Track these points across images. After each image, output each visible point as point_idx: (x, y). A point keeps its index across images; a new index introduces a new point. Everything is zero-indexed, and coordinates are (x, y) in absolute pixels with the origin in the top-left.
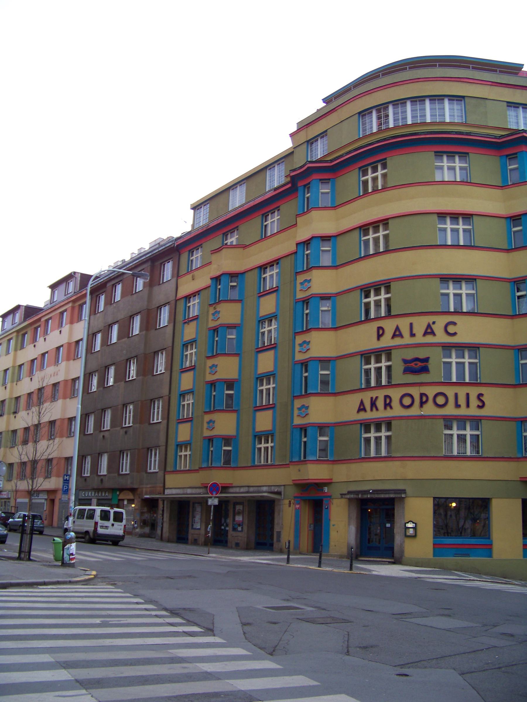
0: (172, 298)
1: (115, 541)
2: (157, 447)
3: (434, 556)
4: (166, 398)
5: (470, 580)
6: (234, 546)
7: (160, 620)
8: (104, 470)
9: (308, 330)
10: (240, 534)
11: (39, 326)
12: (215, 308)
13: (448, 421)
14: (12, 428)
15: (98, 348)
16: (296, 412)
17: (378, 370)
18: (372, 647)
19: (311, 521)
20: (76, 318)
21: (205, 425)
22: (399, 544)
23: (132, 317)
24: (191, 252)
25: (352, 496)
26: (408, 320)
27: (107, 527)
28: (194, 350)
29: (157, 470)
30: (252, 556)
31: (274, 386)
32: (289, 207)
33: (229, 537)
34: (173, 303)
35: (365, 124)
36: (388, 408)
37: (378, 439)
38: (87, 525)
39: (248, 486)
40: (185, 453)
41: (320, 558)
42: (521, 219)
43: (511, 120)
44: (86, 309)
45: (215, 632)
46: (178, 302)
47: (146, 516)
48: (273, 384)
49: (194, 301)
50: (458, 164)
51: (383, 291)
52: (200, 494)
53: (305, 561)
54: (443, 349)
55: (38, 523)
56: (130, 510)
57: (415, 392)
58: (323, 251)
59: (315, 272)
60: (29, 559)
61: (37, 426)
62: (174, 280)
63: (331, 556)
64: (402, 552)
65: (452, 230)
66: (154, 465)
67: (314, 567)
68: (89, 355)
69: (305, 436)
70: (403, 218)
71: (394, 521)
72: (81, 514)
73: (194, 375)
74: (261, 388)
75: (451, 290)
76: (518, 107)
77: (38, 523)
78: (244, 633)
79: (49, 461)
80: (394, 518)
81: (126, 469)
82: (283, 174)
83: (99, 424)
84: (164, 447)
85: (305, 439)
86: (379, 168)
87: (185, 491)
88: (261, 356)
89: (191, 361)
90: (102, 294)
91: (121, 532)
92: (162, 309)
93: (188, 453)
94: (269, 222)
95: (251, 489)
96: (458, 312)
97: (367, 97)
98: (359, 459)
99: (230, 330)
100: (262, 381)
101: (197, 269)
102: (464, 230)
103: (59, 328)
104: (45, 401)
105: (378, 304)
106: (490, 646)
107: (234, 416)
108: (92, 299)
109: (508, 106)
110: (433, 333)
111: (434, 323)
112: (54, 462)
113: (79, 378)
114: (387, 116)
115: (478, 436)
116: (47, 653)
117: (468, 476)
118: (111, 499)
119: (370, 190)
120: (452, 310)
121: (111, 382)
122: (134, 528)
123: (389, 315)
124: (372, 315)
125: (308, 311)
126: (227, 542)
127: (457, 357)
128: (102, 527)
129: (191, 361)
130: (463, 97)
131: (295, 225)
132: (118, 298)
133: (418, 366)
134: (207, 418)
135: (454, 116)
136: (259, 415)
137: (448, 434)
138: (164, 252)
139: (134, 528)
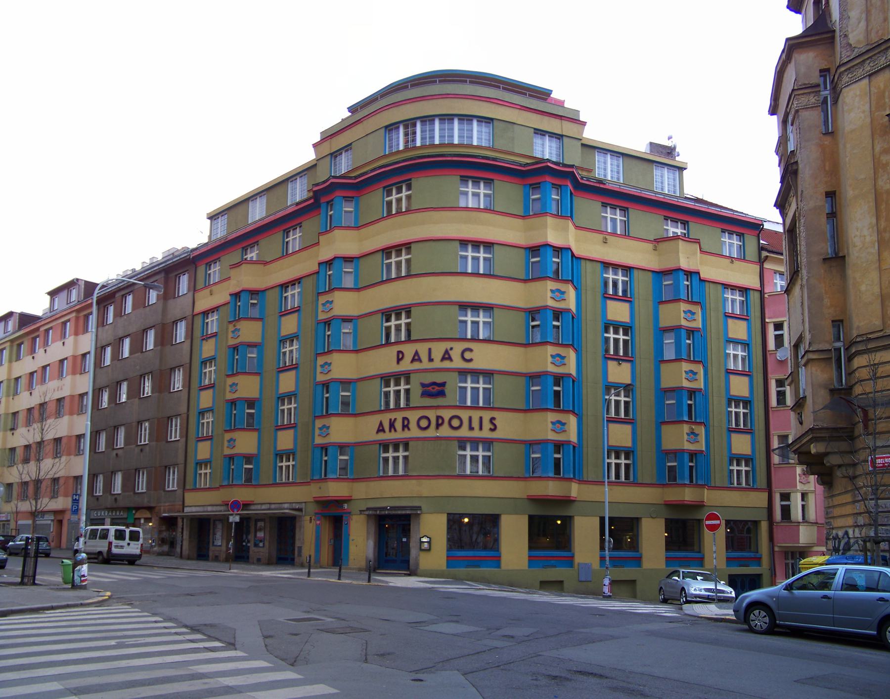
0: (188, 313)
1: (131, 560)
2: (175, 465)
3: (448, 567)
4: (185, 416)
7: (180, 638)
8: (118, 489)
9: (330, 352)
10: (261, 550)
11: (38, 336)
13: (462, 443)
14: (10, 446)
15: (108, 362)
16: (317, 432)
17: (397, 393)
18: (389, 654)
20: (81, 328)
21: (226, 444)
23: (145, 331)
24: (208, 265)
27: (122, 547)
28: (213, 368)
29: (175, 488)
32: (311, 224)
33: (251, 552)
34: (190, 317)
37: (396, 459)
38: (101, 546)
41: (340, 571)
44: (93, 320)
45: (237, 646)
46: (196, 318)
47: (165, 534)
50: (482, 190)
55: (43, 545)
56: (147, 529)
57: (432, 414)
58: (345, 272)
59: (337, 294)
60: (34, 584)
61: (40, 444)
63: (351, 569)
64: (417, 564)
65: (473, 258)
66: (172, 483)
68: (98, 369)
69: (326, 455)
70: (428, 244)
72: (93, 534)
73: (214, 393)
75: (611, 276)
77: (43, 545)
78: (266, 646)
79: (55, 480)
81: (142, 487)
83: (111, 442)
85: (326, 458)
87: (205, 509)
88: (283, 376)
89: (210, 379)
90: (110, 304)
91: (138, 552)
93: (208, 471)
94: (290, 238)
95: (273, 506)
96: (475, 339)
100: (283, 401)
101: (215, 284)
102: (485, 259)
103: (61, 339)
104: (49, 417)
108: (99, 309)
110: (450, 359)
111: (451, 349)
112: (61, 482)
113: (87, 393)
114: (415, 133)
115: (489, 457)
116: (55, 680)
117: (482, 493)
118: (126, 519)
120: (469, 336)
121: (124, 398)
122: (152, 546)
123: (409, 340)
126: (248, 558)
128: (116, 547)
129: (210, 379)
130: (492, 119)
131: (318, 244)
132: (129, 309)
134: (227, 436)
139: (152, 546)
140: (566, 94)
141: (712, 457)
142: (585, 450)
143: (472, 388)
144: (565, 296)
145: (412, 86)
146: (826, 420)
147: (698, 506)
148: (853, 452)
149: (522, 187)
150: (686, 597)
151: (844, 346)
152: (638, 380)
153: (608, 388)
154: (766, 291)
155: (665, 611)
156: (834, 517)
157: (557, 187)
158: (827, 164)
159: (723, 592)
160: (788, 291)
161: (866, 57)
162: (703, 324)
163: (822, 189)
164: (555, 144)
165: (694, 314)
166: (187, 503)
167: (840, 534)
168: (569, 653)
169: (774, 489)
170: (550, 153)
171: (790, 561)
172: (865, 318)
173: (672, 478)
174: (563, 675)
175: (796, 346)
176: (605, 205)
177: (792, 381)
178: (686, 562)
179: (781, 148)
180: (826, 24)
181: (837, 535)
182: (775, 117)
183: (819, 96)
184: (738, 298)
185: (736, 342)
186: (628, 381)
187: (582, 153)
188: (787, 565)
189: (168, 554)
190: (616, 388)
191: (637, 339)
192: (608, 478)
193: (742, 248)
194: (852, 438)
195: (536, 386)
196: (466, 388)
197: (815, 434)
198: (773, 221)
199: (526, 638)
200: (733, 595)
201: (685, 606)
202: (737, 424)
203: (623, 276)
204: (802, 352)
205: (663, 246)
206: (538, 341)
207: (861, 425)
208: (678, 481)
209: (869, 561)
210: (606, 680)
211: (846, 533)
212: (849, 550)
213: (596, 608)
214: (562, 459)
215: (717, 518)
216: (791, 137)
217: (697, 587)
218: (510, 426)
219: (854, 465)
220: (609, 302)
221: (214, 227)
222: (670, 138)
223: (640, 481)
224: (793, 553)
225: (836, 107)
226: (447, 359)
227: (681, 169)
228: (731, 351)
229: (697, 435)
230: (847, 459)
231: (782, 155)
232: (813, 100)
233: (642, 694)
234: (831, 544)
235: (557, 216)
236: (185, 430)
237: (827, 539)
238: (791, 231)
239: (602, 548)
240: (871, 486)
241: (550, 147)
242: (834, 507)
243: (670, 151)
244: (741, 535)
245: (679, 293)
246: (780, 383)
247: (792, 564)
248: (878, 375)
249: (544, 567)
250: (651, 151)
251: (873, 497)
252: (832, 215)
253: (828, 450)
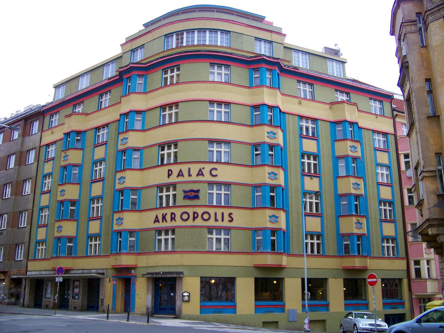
0: (37, 145)
3: (201, 313)
4: (31, 211)
6: (73, 309)
9: (125, 170)
10: (77, 301)
12: (65, 153)
13: (210, 230)
16: (115, 222)
17: (168, 197)
19: (123, 292)
21: (56, 229)
23: (9, 156)
24: (52, 116)
26: (188, 166)
29: (22, 259)
30: (84, 315)
31: (102, 204)
32: (117, 91)
33: (70, 303)
37: (166, 240)
39: (83, 269)
40: (42, 248)
41: (128, 316)
46: (41, 148)
47: (13, 290)
48: (101, 203)
49: (52, 148)
50: (223, 71)
51: (173, 147)
52: (51, 274)
53: (119, 318)
57: (190, 211)
59: (130, 133)
62: (40, 133)
63: (136, 314)
64: (181, 311)
65: (218, 112)
66: (20, 256)
67: (125, 321)
69: (120, 237)
74: (93, 206)
75: (215, 148)
82: (115, 69)
84: (28, 243)
85: (120, 239)
86: (175, 70)
87: (41, 273)
88: (94, 185)
92: (31, 152)
93: (44, 247)
94: (103, 99)
95: (85, 271)
96: (219, 162)
99: (75, 168)
102: (225, 112)
107: (75, 223)
111: (203, 168)
114: (183, 38)
115: (228, 239)
117: (221, 264)
119: (168, 84)
122: (4, 299)
123: (176, 163)
124: (165, 162)
125: (125, 158)
126: (68, 306)
127: (217, 190)
130: (230, 32)
134: (57, 224)
136: (91, 223)
137: (210, 238)
138: (33, 115)
139: (4, 299)
140: (273, 18)
142: (291, 234)
144: (276, 136)
146: (436, 214)
147: (364, 270)
150: (357, 329)
152: (323, 189)
153: (305, 194)
154: (398, 135)
160: (409, 135)
161: (441, 7)
162: (362, 155)
163: (423, 77)
164: (267, 45)
166: (29, 269)
170: (265, 51)
171: (422, 305)
173: (346, 251)
175: (416, 168)
177: (415, 190)
178: (357, 307)
182: (394, 36)
183: (416, 26)
184: (382, 139)
185: (382, 165)
186: (318, 190)
189: (14, 304)
192: (306, 252)
193: (382, 109)
195: (259, 192)
196: (213, 194)
197: (430, 222)
202: (385, 217)
203: (312, 124)
205: (335, 106)
208: (351, 254)
214: (276, 240)
215: (375, 277)
216: (404, 47)
218: (242, 219)
220: (304, 140)
221: (57, 92)
223: (327, 254)
225: (427, 32)
226: (200, 175)
227: (344, 63)
228: (379, 171)
229: (361, 224)
231: (399, 58)
232: (414, 29)
236: (30, 220)
238: (408, 100)
239: (303, 299)
241: (265, 47)
243: (337, 53)
244: (391, 288)
246: (409, 191)
250: (326, 52)
252: (430, 92)
253: (439, 233)
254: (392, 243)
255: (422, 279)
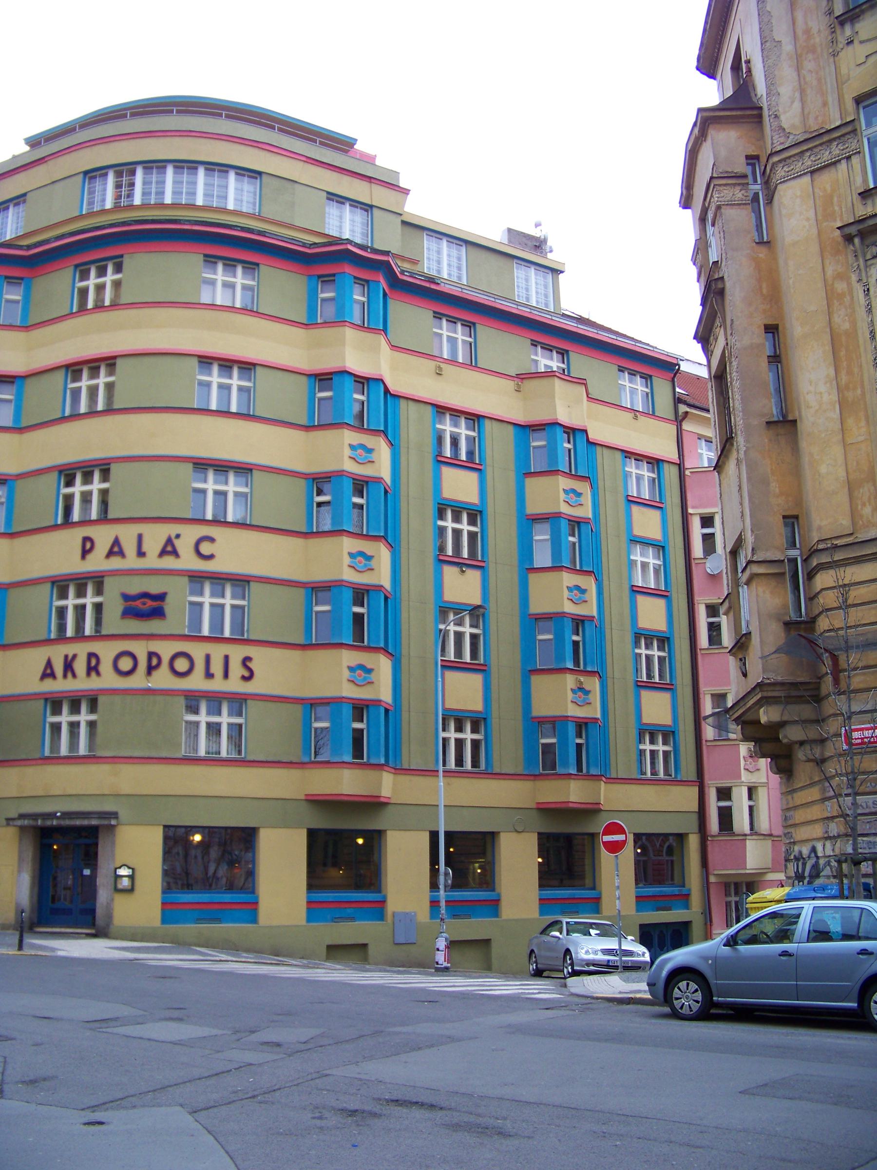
3: (164, 921)
5: (221, 961)
13: (192, 701)
17: (80, 610)
18: (45, 1079)
22: (105, 904)
25: (26, 822)
26: (134, 529)
35: (94, 192)
36: (93, 674)
37: (74, 726)
42: (331, 379)
43: (331, 221)
50: (240, 278)
51: (97, 476)
54: (190, 581)
57: (140, 649)
64: (109, 917)
65: (221, 386)
70: (140, 359)
71: (96, 865)
75: (211, 484)
76: (343, 203)
80: (97, 861)
96: (219, 522)
97: (101, 148)
98: (41, 759)
102: (240, 389)
105: (86, 498)
106: (242, 1065)
109: (328, 199)
111: (178, 536)
114: (132, 185)
115: (240, 726)
117: (220, 791)
119: (90, 305)
123: (104, 518)
124: (76, 516)
127: (213, 595)
130: (260, 173)
133: (147, 607)
135: (242, 201)
140: (377, 144)
141: (612, 730)
142: (405, 715)
143: (212, 605)
145: (133, 115)
146: (781, 671)
147: (591, 811)
148: (819, 721)
149: (305, 278)
151: (801, 555)
152: (492, 599)
153: (444, 611)
154: (687, 465)
155: (540, 990)
156: (795, 825)
157: (364, 283)
158: (764, 285)
159: (630, 953)
160: (718, 466)
161: (805, 147)
162: (594, 513)
163: (760, 320)
164: (359, 216)
165: (579, 495)
167: (805, 851)
168: (374, 1069)
169: (708, 781)
170: (352, 231)
171: (733, 899)
172: (827, 518)
173: (548, 763)
174: (367, 1108)
175: (734, 554)
176: (438, 316)
177: (730, 608)
178: (571, 906)
179: (700, 256)
180: (750, 98)
181: (800, 853)
182: (689, 211)
183: (747, 190)
184: (646, 472)
185: (645, 543)
186: (478, 602)
187: (402, 230)
188: (728, 904)
190: (457, 611)
191: (491, 532)
192: (444, 764)
193: (650, 397)
194: (818, 699)
197: (766, 694)
198: (694, 361)
199: (303, 1047)
200: (647, 958)
201: (571, 981)
202: (649, 675)
203: (468, 428)
204: (742, 563)
205: (529, 385)
206: (327, 527)
207: (829, 678)
208: (559, 770)
209: (846, 892)
210: (440, 1113)
211: (814, 850)
212: (818, 876)
213: (423, 990)
214: (367, 730)
215: (621, 831)
217: (590, 947)
218: (276, 673)
219: (822, 741)
220: (446, 471)
222: (537, 225)
224: (736, 885)
225: (771, 208)
227: (556, 272)
229: (587, 693)
230: (812, 733)
232: (740, 195)
233: (500, 1133)
234: (791, 868)
235: (361, 327)
237: (787, 860)
238: (720, 377)
239: (434, 886)
240: (847, 774)
241: (352, 221)
242: (795, 808)
244: (658, 858)
245: (557, 462)
246: (712, 610)
247: (736, 903)
248: (850, 602)
249: (335, 920)
250: (510, 241)
251: (849, 791)
252: (775, 359)
253: (785, 718)
254: (665, 743)
255: (734, 834)
